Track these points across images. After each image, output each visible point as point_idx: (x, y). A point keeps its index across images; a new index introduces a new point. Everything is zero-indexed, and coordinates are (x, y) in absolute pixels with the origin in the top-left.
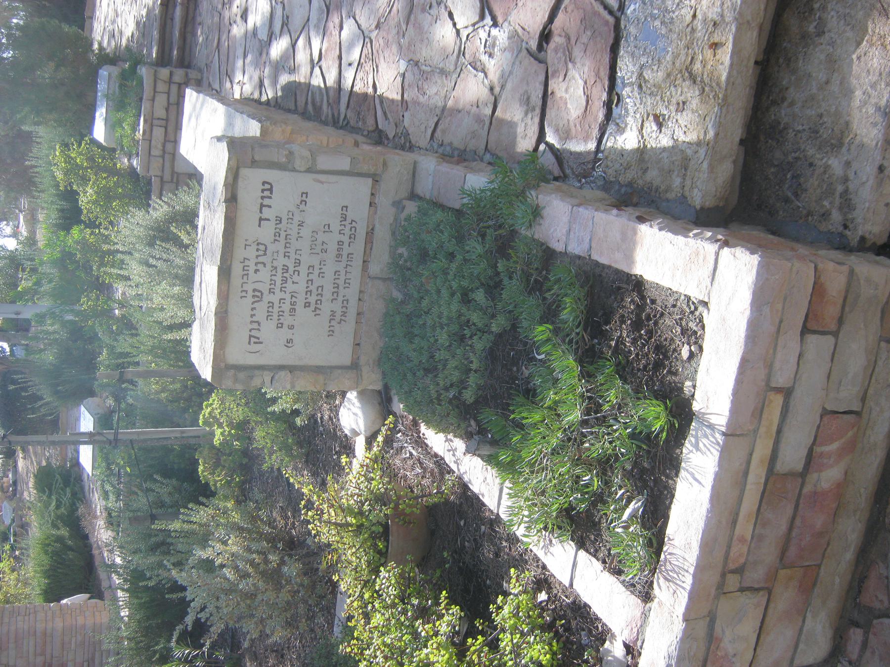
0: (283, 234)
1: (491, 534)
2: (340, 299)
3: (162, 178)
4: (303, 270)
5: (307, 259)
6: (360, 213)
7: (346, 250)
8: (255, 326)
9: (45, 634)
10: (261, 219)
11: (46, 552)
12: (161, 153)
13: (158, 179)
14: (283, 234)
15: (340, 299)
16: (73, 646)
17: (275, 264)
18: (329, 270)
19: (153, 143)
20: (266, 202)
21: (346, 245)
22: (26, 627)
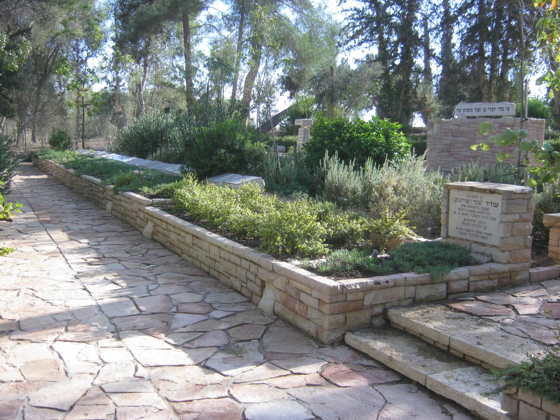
2: (466, 232)
4: (474, 218)
5: (477, 219)
7: (480, 235)
15: (466, 232)
18: (474, 228)
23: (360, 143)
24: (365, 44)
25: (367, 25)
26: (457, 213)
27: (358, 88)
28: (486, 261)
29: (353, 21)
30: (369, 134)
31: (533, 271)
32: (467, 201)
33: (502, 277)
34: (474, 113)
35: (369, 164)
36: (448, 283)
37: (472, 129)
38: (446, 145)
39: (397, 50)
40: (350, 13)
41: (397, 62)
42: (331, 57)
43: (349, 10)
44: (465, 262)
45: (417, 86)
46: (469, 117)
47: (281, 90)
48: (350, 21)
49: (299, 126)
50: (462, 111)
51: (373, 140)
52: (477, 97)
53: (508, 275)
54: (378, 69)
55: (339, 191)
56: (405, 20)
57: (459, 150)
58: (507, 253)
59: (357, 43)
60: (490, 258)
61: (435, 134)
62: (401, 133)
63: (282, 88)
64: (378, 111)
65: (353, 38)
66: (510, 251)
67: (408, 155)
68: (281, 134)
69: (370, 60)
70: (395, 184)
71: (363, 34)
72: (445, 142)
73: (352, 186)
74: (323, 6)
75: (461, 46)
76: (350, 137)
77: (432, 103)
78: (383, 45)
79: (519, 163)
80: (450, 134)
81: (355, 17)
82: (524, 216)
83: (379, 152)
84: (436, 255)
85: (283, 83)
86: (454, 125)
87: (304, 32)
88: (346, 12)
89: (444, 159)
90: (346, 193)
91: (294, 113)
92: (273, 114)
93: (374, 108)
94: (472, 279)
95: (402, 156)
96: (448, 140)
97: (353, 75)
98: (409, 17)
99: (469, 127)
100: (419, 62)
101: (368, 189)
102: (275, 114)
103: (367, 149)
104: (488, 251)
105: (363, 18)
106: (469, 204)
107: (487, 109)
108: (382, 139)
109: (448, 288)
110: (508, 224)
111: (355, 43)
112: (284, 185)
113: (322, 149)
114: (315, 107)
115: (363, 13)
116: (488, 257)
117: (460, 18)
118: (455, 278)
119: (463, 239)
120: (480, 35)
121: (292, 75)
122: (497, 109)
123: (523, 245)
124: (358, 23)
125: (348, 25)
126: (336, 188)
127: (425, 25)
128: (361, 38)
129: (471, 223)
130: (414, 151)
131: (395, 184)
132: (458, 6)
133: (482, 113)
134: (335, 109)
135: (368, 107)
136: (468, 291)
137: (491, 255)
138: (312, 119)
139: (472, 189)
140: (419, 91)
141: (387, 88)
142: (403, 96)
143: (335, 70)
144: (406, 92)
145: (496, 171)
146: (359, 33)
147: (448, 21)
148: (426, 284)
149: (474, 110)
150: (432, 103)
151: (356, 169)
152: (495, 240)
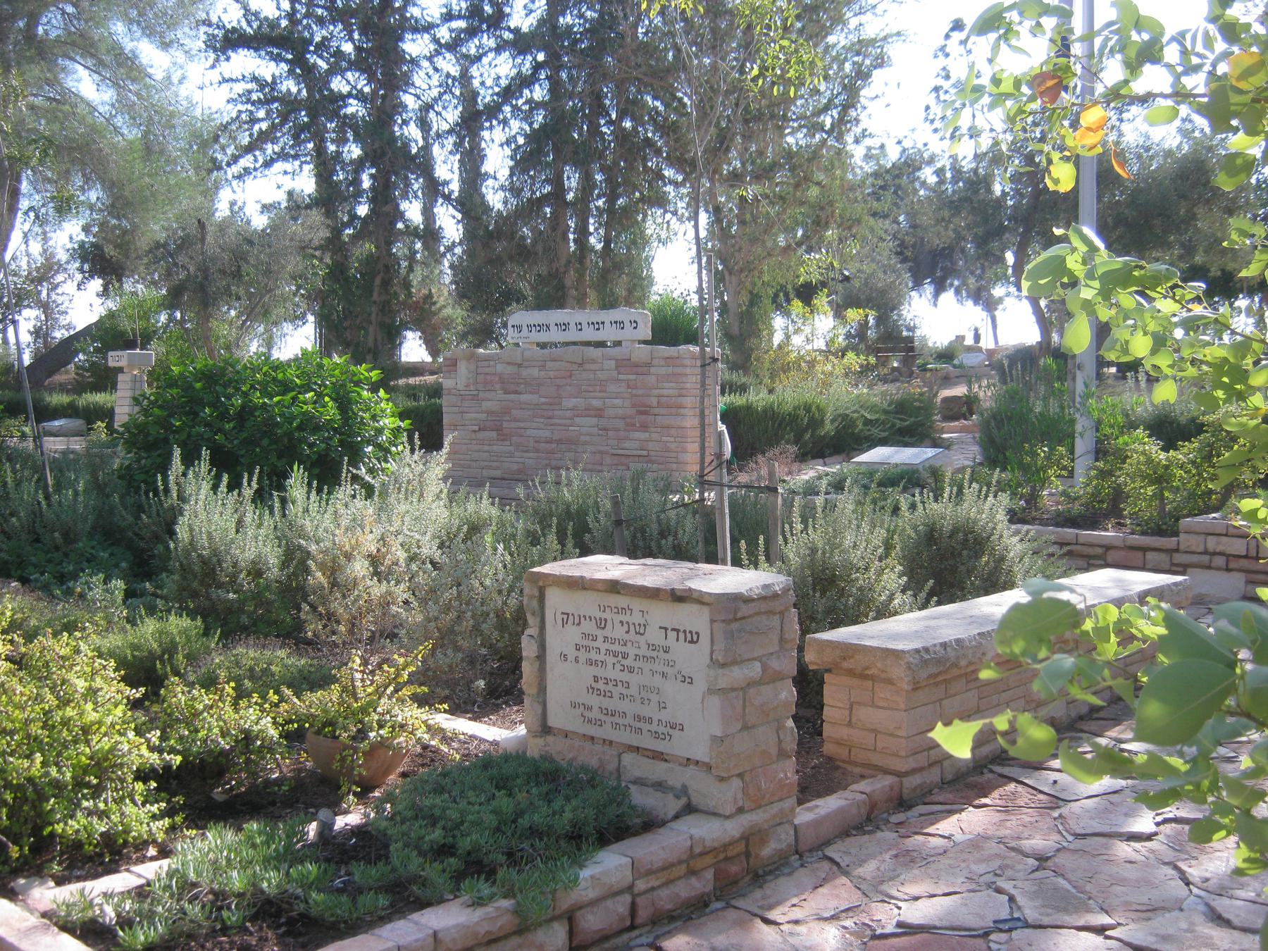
0: (654, 654)
1: (335, 849)
2: (603, 717)
3: (1177, 550)
4: (625, 676)
5: (635, 679)
6: (679, 746)
7: (645, 727)
8: (577, 621)
9: (680, 407)
10: (666, 629)
11: (795, 408)
12: (1211, 550)
13: (1173, 546)
14: (654, 654)
15: (603, 717)
16: (665, 439)
17: (629, 644)
18: (625, 706)
19: (1224, 539)
20: (682, 635)
21: (649, 727)
22: (688, 385)
23: (270, 424)
24: (279, 166)
25: (285, 118)
26: (571, 658)
27: (268, 272)
28: (671, 813)
29: (249, 107)
30: (294, 399)
31: (804, 816)
32: (602, 624)
33: (727, 859)
34: (555, 336)
35: (297, 484)
36: (570, 917)
37: (551, 374)
38: (489, 413)
39: (361, 182)
40: (240, 88)
41: (363, 210)
42: (200, 199)
43: (237, 80)
44: (618, 827)
45: (411, 269)
46: (543, 346)
47: (79, 277)
48: (240, 107)
49: (121, 370)
50: (525, 328)
51: (306, 413)
52: (552, 295)
53: (741, 847)
54: (315, 227)
55: (214, 570)
56: (378, 109)
57: (522, 425)
58: (736, 783)
59: (261, 160)
60: (684, 801)
61: (460, 386)
62: (382, 393)
63: (81, 270)
64: (319, 324)
65: (249, 149)
66: (740, 776)
67: (402, 448)
68: (80, 387)
69: (296, 205)
70: (373, 549)
71: (274, 141)
72: (487, 405)
73: (250, 554)
74: (175, 80)
75: (511, 175)
76: (243, 407)
77: (444, 306)
78: (325, 167)
79: (702, 476)
80: (498, 386)
81: (254, 97)
82: (775, 664)
83: (323, 446)
84: (524, 822)
85: (84, 259)
86: (508, 363)
87: (130, 137)
88: (230, 84)
89: (486, 448)
90: (234, 577)
91: (108, 335)
92: (59, 335)
93: (311, 318)
94: (641, 885)
95: (384, 452)
96: (494, 401)
97: (256, 241)
98: (387, 102)
99: (542, 368)
100: (413, 211)
101: (295, 558)
102: (67, 335)
103: (291, 439)
104: (678, 776)
105: (274, 99)
106: (608, 632)
107: (585, 326)
108: (330, 411)
109: (571, 933)
110: (734, 694)
111: (256, 160)
112: (57, 548)
113: (166, 441)
114: (163, 318)
115: (273, 89)
116: (678, 797)
117: (507, 109)
118: (592, 894)
119: (592, 738)
120: (557, 150)
121: (104, 239)
122: (607, 324)
123: (774, 751)
124: (261, 114)
125: (238, 117)
126: (204, 561)
127: (424, 125)
128: (270, 148)
129: (616, 691)
130: (417, 442)
131: (373, 549)
132: (504, 82)
133: (572, 335)
134: (213, 324)
135: (296, 318)
136: (632, 927)
137: (684, 790)
138: (153, 352)
139: (614, 587)
140: (415, 279)
141: (338, 272)
142: (380, 294)
143: (210, 229)
144: (386, 284)
145: (635, 490)
146: (264, 137)
147: (473, 120)
148: (506, 937)
149: (553, 328)
150: (444, 306)
151: (260, 497)
152: (695, 742)
